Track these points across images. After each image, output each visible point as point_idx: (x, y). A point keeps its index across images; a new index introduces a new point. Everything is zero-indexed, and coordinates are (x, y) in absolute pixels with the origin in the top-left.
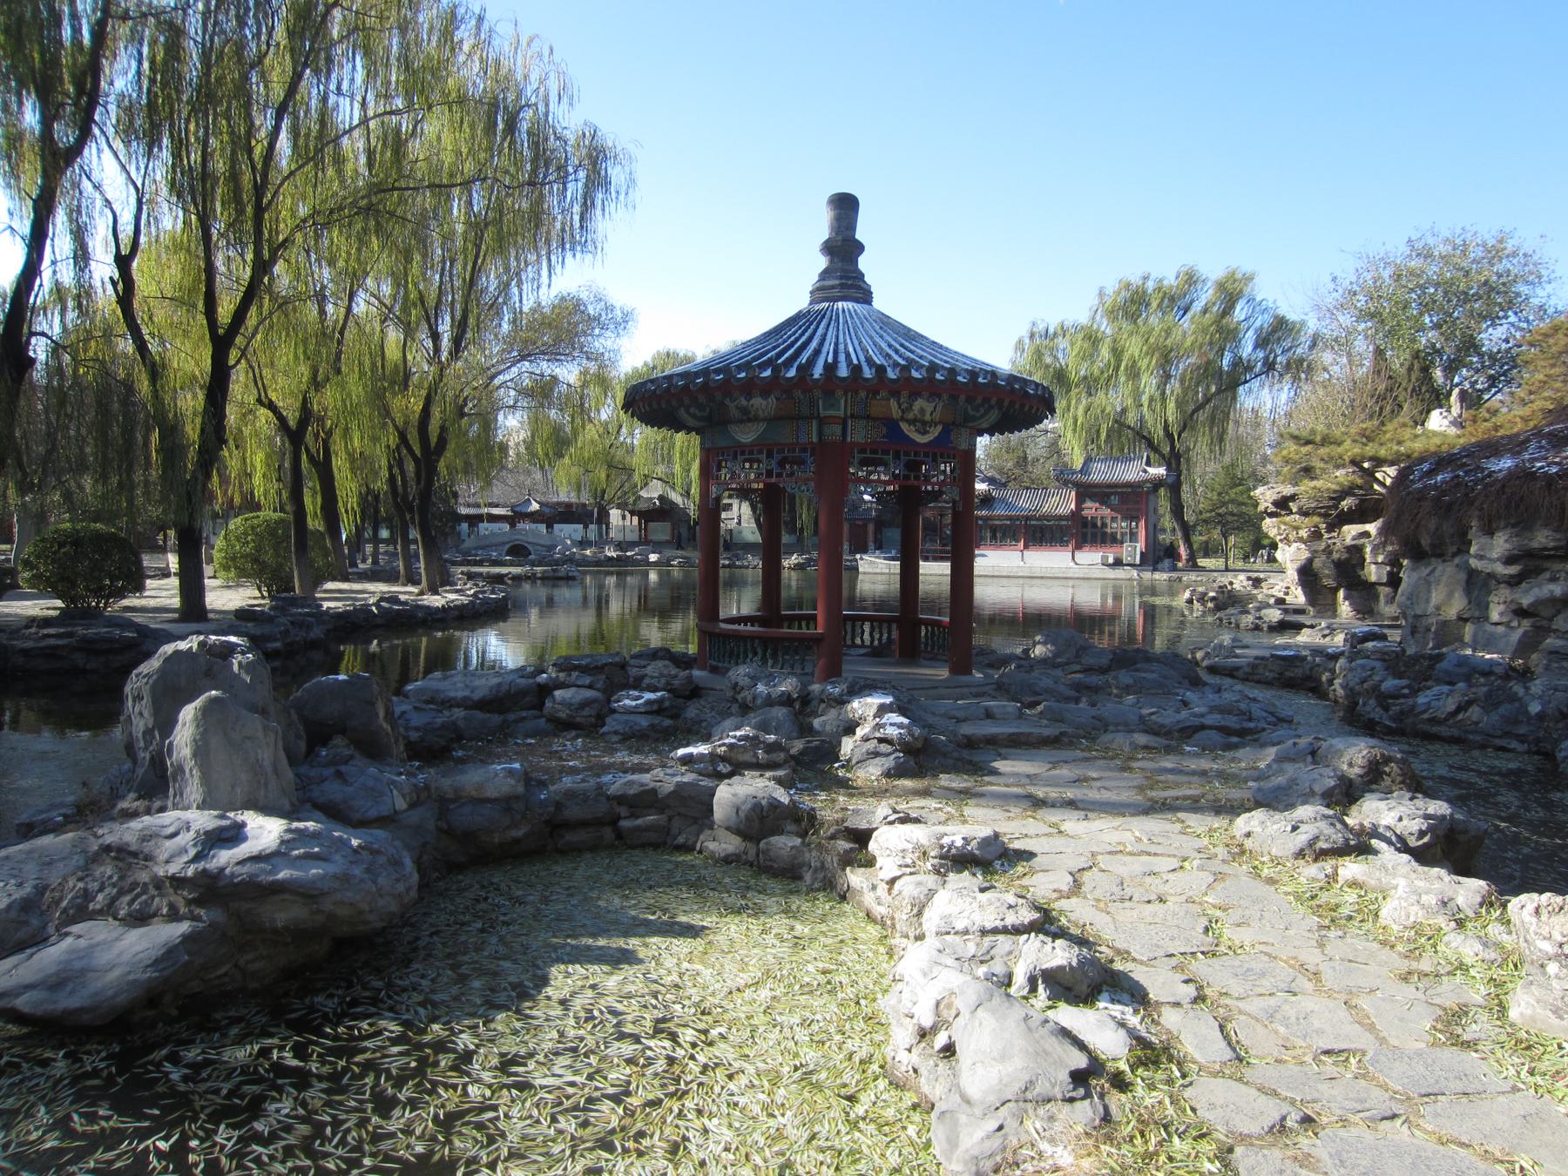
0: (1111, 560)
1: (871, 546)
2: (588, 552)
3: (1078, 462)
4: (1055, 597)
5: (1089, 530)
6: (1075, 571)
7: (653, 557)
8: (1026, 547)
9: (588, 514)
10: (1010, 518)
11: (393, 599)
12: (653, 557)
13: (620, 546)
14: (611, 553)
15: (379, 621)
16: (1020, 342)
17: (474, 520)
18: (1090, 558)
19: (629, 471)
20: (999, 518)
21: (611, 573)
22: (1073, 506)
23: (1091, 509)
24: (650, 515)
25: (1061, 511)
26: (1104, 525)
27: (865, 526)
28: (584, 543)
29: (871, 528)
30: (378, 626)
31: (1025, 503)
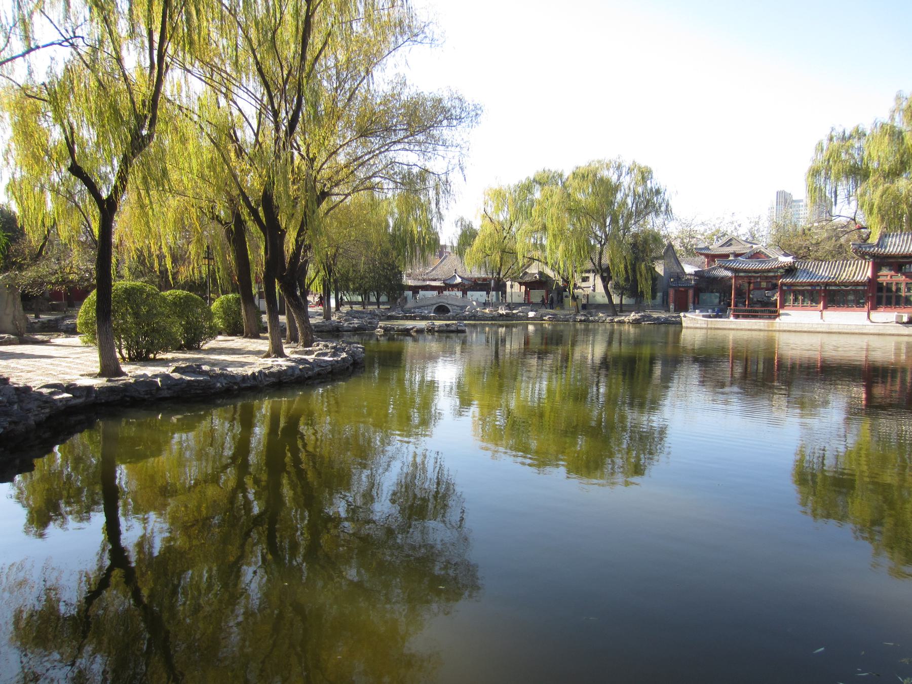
0: (905, 319)
1: (691, 306)
2: (487, 311)
3: (874, 239)
4: (850, 350)
5: (884, 294)
6: (871, 328)
7: (531, 314)
8: (825, 307)
9: (494, 285)
10: (811, 284)
11: (145, 375)
12: (531, 314)
13: (509, 306)
14: (503, 311)
15: (166, 393)
16: (820, 144)
17: (415, 290)
18: (885, 317)
19: (513, 253)
20: (802, 284)
21: (502, 326)
22: (869, 274)
23: (886, 276)
24: (531, 285)
25: (859, 278)
26: (898, 290)
27: (686, 292)
28: (486, 304)
29: (691, 293)
30: (164, 399)
31: (825, 272)
